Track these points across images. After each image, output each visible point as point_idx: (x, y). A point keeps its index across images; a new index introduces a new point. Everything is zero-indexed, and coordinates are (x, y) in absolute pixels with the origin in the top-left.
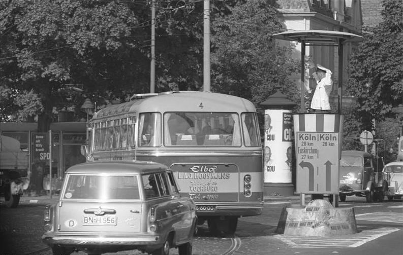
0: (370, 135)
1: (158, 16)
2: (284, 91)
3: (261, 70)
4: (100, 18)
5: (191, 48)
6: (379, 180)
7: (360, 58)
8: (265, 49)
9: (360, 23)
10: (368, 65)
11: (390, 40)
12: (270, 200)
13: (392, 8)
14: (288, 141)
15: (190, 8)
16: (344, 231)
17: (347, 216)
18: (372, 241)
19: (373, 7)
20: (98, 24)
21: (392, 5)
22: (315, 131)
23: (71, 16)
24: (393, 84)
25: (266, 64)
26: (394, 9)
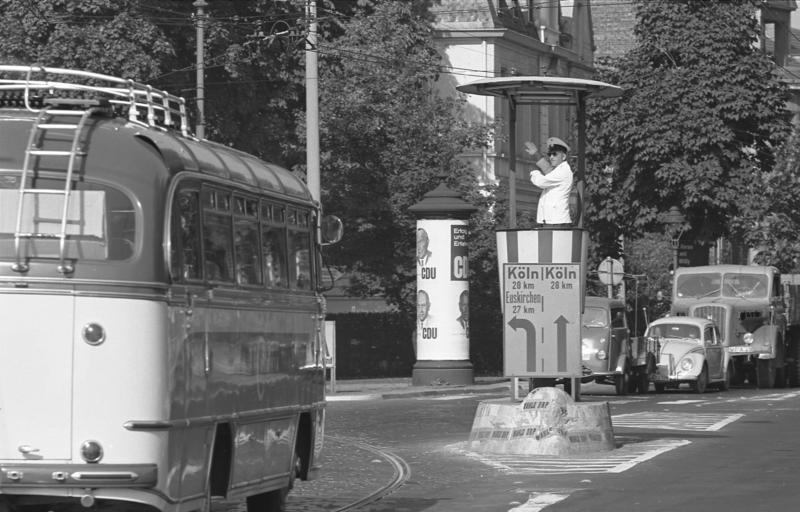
0: (619, 265)
1: (209, 41)
2: (452, 183)
3: (407, 144)
4: (101, 44)
5: (272, 101)
6: (639, 352)
7: (595, 119)
8: (414, 102)
9: (589, 48)
10: (609, 131)
11: (651, 82)
12: (435, 394)
13: (654, 20)
14: (462, 279)
15: (298, 34)
16: (593, 445)
17: (598, 416)
18: (646, 461)
19: (611, 16)
20: (98, 55)
21: (654, 16)
22: (570, 262)
23: (44, 40)
24: (659, 168)
25: (417, 132)
26: (659, 23)
